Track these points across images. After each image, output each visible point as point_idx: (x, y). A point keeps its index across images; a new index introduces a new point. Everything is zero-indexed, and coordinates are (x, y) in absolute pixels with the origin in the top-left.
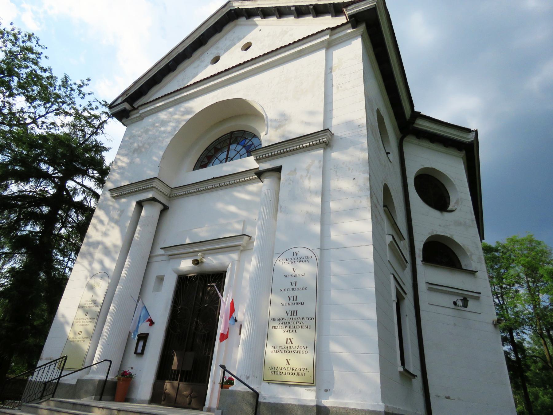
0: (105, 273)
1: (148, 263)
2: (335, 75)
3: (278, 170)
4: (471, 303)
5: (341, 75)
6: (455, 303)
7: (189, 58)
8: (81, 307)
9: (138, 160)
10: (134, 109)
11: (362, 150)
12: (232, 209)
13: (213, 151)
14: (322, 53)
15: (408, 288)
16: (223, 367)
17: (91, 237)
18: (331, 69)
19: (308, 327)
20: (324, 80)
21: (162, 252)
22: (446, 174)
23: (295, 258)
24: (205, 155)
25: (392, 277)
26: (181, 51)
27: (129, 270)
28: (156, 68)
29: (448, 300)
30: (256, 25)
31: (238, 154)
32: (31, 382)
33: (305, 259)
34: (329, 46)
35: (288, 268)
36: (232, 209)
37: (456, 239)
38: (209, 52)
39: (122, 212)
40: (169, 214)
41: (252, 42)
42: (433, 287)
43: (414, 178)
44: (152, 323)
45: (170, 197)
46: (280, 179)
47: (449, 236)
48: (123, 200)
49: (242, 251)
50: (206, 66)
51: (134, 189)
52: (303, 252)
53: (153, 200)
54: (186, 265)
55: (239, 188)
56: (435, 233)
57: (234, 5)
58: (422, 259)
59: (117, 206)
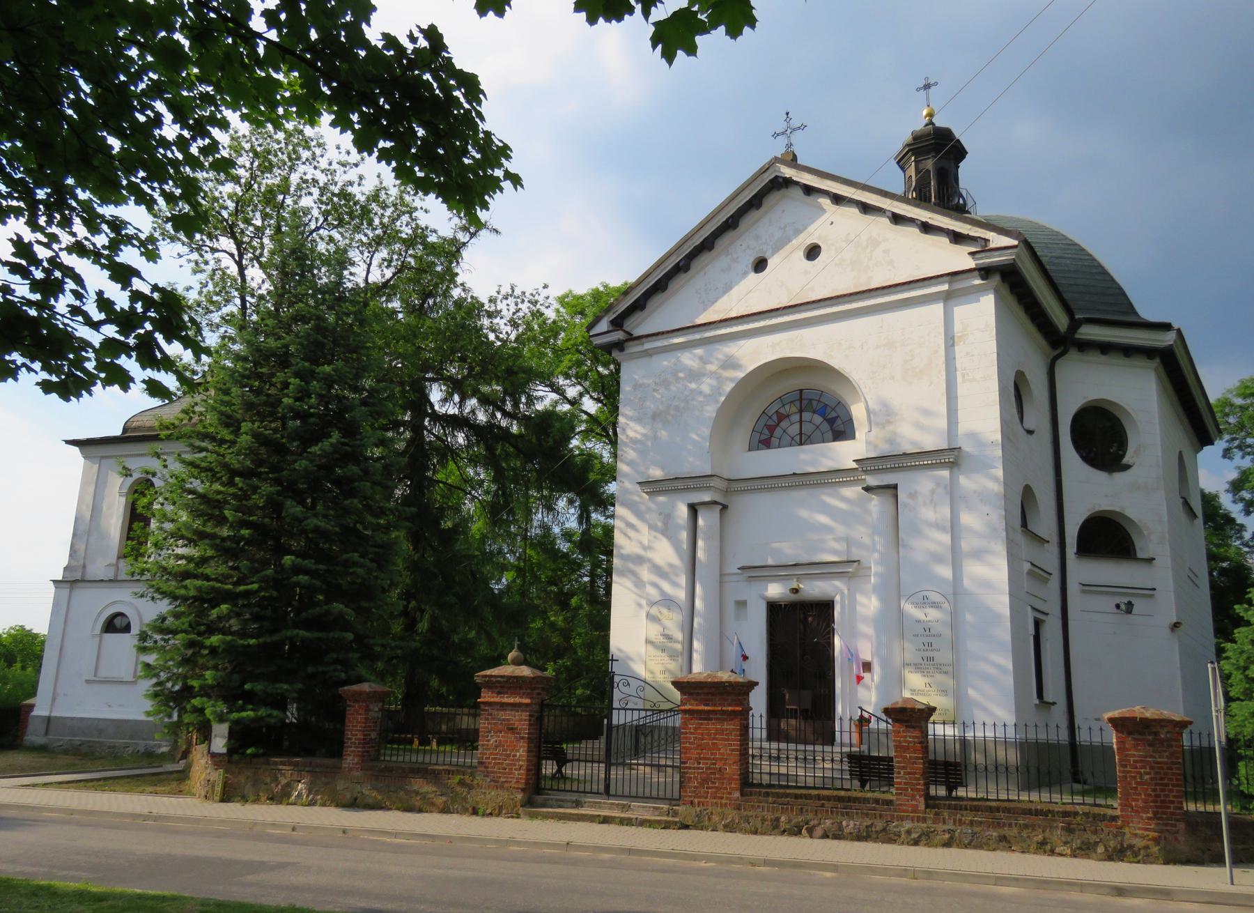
0: (668, 601)
2: (959, 350)
4: (1139, 605)
5: (968, 354)
6: (1118, 606)
8: (648, 642)
9: (663, 434)
10: (631, 338)
11: (996, 479)
12: (823, 519)
15: (1054, 608)
16: (860, 708)
17: (621, 547)
18: (953, 338)
19: (946, 673)
20: (944, 359)
22: (1126, 407)
23: (925, 602)
24: (763, 424)
25: (1029, 608)
26: (698, 243)
27: (704, 599)
28: (659, 270)
29: (1108, 603)
30: (823, 211)
31: (818, 431)
32: (624, 729)
33: (935, 605)
35: (918, 614)
36: (823, 519)
37: (1129, 513)
38: (743, 246)
39: (667, 517)
41: (820, 244)
42: (1087, 588)
46: (896, 497)
47: (1118, 510)
48: (661, 499)
49: (850, 577)
50: (745, 274)
52: (935, 597)
54: (775, 590)
55: (829, 490)
56: (1097, 509)
57: (782, 170)
58: (1075, 550)
59: (652, 505)
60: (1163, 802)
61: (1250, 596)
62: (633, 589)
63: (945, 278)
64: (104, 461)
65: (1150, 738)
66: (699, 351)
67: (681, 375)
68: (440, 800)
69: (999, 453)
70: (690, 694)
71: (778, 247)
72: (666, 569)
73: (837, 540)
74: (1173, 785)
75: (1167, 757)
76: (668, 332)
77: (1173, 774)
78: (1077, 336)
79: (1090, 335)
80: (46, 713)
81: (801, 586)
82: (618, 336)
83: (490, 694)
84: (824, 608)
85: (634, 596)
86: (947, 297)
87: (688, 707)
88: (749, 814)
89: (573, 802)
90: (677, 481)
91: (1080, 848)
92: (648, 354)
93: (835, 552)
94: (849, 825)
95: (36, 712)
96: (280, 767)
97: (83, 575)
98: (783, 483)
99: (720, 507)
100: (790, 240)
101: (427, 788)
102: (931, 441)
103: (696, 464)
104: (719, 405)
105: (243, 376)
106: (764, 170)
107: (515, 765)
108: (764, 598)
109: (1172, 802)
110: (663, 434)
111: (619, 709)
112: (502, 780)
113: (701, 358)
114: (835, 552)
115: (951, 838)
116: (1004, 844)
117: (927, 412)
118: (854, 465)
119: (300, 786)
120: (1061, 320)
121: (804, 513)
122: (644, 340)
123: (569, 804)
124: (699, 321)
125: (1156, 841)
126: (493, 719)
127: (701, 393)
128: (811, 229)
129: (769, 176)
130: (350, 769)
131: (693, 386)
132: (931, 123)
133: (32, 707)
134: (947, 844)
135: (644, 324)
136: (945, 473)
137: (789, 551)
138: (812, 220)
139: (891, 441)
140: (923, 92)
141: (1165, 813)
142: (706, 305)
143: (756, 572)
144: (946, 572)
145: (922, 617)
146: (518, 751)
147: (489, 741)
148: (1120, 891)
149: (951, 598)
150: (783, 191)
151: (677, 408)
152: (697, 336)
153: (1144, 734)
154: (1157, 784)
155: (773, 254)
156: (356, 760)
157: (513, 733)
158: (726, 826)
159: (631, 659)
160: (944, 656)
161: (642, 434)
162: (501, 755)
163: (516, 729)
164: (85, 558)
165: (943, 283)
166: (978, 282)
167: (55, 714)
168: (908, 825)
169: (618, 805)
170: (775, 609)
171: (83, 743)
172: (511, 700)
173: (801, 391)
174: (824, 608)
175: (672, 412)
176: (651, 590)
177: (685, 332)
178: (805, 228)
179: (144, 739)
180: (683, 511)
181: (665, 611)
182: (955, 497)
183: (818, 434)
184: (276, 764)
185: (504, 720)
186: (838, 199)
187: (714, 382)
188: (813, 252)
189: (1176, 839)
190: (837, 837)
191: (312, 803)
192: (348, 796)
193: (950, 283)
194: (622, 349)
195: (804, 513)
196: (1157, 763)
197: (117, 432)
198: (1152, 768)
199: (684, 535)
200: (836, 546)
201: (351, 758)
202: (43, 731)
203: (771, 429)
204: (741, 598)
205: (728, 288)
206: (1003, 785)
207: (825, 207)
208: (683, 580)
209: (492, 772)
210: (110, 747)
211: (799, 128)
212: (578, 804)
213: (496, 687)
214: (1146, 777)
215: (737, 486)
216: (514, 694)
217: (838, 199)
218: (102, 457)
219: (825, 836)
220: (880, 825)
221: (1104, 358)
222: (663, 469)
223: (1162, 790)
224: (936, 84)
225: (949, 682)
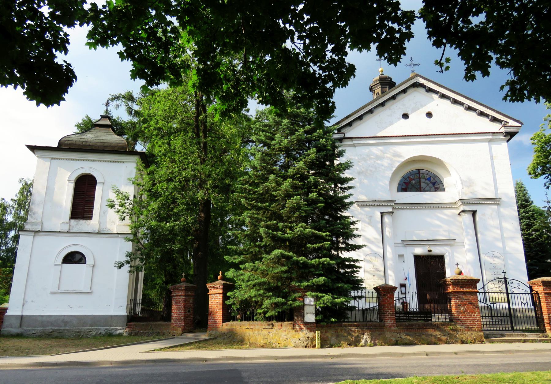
9: (365, 181)
12: (438, 222)
23: (493, 256)
30: (433, 99)
33: (498, 257)
35: (491, 260)
36: (438, 222)
48: (367, 209)
50: (399, 119)
52: (496, 254)
54: (420, 251)
64: (53, 161)
66: (381, 148)
68: (444, 338)
70: (546, 286)
71: (414, 110)
72: (374, 240)
73: (445, 231)
80: (19, 313)
83: (457, 288)
84: (441, 259)
86: (490, 141)
87: (546, 291)
89: (500, 335)
90: (376, 202)
92: (354, 146)
95: (9, 313)
96: (350, 328)
97: (42, 229)
100: (419, 109)
101: (438, 333)
104: (393, 172)
105: (204, 123)
106: (412, 78)
107: (475, 320)
111: (511, 294)
112: (470, 327)
113: (381, 151)
119: (365, 337)
121: (429, 220)
122: (353, 139)
123: (499, 336)
126: (460, 299)
127: (383, 165)
128: (428, 105)
129: (413, 81)
130: (390, 327)
131: (379, 162)
133: (6, 310)
135: (350, 133)
136: (496, 207)
137: (424, 235)
139: (472, 193)
143: (406, 243)
144: (500, 245)
145: (493, 262)
146: (475, 313)
147: (460, 309)
150: (416, 89)
151: (371, 171)
155: (412, 112)
156: (392, 322)
157: (472, 305)
162: (467, 315)
163: (473, 303)
164: (42, 218)
166: (502, 137)
167: (24, 314)
169: (520, 334)
170: (418, 259)
171: (54, 331)
172: (468, 290)
173: (419, 170)
174: (441, 259)
175: (369, 172)
177: (375, 138)
178: (425, 105)
179: (103, 326)
181: (374, 258)
182: (501, 217)
183: (428, 188)
184: (345, 326)
185: (466, 299)
187: (389, 162)
191: (375, 345)
192: (394, 339)
195: (429, 220)
197: (56, 145)
201: (390, 321)
202: (18, 324)
204: (401, 253)
205: (391, 123)
206: (523, 325)
207: (434, 98)
209: (465, 324)
210: (76, 332)
211: (417, 65)
212: (503, 335)
213: (459, 285)
216: (469, 288)
218: (52, 159)
222: (366, 196)
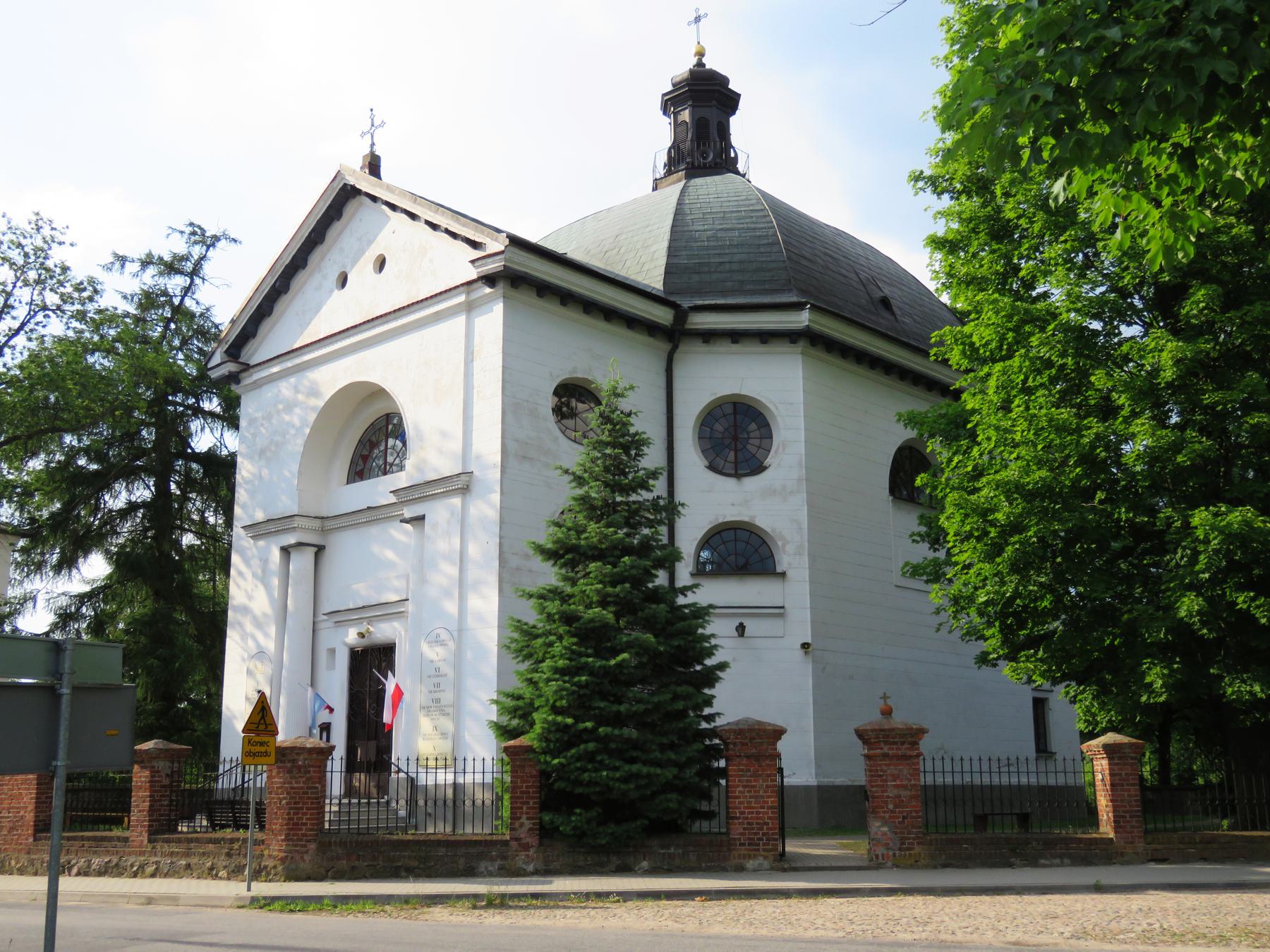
1: (314, 631)
3: (422, 518)
7: (304, 268)
10: (247, 367)
13: (361, 462)
14: (461, 319)
21: (325, 617)
22: (759, 398)
28: (258, 295)
34: (470, 308)
38: (326, 263)
39: (265, 561)
40: (328, 555)
43: (744, 392)
44: (331, 710)
45: (324, 531)
47: (746, 519)
48: (261, 543)
50: (331, 291)
51: (272, 527)
53: (300, 545)
56: (721, 520)
58: (691, 569)
60: (296, 824)
61: (539, 617)
62: (239, 641)
63: (461, 289)
65: (289, 765)
67: (281, 407)
69: (497, 474)
71: (355, 261)
74: (307, 809)
75: (304, 782)
76: (264, 362)
77: (308, 798)
78: (688, 326)
79: (703, 324)
81: (371, 629)
82: (231, 367)
85: (240, 649)
88: (34, 857)
91: (233, 871)
92: (258, 385)
93: (396, 591)
94: (96, 862)
98: (362, 518)
99: (316, 549)
102: (447, 468)
103: (287, 505)
108: (346, 644)
109: (306, 824)
110: (265, 472)
114: (396, 591)
115: (157, 869)
116: (189, 872)
117: (444, 434)
118: (393, 499)
120: (663, 315)
124: (296, 346)
125: (283, 860)
131: (287, 418)
132: (700, 64)
134: (153, 875)
136: (456, 501)
138: (380, 228)
140: (694, 26)
141: (297, 835)
142: (304, 325)
143: (342, 617)
148: (150, 901)
149: (455, 634)
152: (289, 364)
153: (284, 762)
154: (290, 809)
158: (18, 869)
159: (235, 717)
160: (447, 697)
161: (251, 473)
165: (460, 293)
166: (488, 290)
168: (132, 859)
176: (251, 643)
180: (276, 554)
181: (259, 665)
186: (393, 207)
188: (381, 264)
189: (302, 858)
190: (86, 874)
193: (468, 293)
194: (238, 382)
196: (292, 788)
198: (288, 793)
199: (275, 582)
200: (397, 583)
203: (365, 458)
208: (272, 630)
214: (284, 802)
215: (328, 524)
217: (393, 207)
219: (78, 874)
220: (115, 860)
221: (735, 347)
223: (295, 814)
224: (689, 24)
225: (448, 725)
